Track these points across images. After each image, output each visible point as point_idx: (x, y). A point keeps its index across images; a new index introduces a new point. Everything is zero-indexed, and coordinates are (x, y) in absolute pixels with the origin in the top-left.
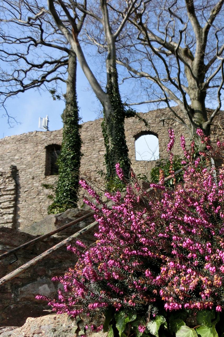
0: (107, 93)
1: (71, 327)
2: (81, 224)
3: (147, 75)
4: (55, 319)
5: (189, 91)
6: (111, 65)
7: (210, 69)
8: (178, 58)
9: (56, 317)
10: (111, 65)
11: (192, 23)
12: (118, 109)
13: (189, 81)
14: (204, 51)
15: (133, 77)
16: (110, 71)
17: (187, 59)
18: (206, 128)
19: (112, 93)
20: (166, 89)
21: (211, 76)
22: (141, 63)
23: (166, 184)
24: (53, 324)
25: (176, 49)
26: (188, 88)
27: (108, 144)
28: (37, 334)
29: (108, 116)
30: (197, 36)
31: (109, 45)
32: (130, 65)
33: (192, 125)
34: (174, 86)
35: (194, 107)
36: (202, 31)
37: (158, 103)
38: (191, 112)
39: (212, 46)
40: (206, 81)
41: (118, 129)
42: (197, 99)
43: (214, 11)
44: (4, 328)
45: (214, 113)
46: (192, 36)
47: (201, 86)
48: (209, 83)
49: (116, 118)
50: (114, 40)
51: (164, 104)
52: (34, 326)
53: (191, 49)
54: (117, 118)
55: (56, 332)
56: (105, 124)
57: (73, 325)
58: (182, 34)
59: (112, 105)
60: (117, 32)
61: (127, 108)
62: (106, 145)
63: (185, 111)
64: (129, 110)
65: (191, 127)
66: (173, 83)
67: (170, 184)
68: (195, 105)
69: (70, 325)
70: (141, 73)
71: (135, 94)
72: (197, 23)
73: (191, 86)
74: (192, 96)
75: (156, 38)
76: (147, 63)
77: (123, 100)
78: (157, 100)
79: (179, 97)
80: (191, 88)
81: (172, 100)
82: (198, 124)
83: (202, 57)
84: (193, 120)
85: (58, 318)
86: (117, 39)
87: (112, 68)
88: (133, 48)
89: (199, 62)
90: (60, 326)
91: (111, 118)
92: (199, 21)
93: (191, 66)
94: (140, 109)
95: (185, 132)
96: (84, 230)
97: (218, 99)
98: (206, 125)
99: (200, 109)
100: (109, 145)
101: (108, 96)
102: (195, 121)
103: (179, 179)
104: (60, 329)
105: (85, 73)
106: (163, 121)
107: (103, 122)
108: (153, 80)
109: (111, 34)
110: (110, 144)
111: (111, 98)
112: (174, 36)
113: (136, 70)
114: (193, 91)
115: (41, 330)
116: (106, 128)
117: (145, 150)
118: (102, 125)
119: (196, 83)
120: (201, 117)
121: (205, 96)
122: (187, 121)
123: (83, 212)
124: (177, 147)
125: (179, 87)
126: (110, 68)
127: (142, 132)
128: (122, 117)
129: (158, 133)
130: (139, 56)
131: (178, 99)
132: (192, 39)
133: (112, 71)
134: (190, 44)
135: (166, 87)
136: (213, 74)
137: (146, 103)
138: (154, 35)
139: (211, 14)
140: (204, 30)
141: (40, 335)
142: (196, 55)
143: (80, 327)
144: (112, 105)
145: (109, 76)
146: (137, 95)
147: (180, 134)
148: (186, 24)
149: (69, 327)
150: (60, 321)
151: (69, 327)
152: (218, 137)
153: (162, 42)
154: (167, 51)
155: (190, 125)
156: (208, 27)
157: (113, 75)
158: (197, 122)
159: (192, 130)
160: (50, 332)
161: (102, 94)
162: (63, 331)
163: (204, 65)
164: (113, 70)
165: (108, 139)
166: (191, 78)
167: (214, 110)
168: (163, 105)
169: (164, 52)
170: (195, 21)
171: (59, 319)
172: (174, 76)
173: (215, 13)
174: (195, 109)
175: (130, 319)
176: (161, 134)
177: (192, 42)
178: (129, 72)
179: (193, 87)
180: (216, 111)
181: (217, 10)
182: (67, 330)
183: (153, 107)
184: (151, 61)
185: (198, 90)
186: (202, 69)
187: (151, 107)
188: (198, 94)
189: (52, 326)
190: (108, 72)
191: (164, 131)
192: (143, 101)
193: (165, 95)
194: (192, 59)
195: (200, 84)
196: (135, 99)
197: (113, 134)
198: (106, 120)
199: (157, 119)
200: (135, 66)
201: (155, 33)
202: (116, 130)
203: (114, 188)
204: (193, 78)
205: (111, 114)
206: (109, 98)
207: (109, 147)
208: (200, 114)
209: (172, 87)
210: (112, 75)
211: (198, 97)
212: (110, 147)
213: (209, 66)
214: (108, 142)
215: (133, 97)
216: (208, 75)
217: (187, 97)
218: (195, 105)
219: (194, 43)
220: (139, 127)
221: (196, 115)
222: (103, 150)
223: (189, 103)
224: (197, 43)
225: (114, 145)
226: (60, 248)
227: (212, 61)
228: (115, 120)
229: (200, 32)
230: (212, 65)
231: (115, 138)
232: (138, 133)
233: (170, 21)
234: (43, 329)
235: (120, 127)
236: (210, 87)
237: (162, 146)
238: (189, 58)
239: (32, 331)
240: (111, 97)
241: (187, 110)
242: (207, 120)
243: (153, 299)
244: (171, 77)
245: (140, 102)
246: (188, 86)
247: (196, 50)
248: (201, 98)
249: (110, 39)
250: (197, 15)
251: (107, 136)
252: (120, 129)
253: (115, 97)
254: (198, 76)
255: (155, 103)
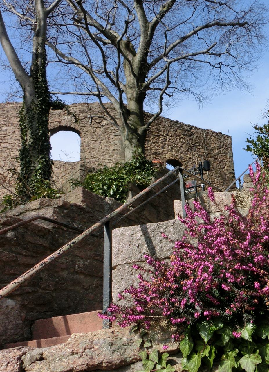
0: (31, 76)
1: (134, 340)
2: (8, 234)
3: (77, 62)
4: (113, 333)
5: (126, 89)
6: (39, 44)
7: (152, 70)
8: (120, 51)
9: (114, 331)
10: (39, 44)
11: (138, 14)
12: (42, 97)
13: (127, 78)
14: (149, 49)
15: (60, 61)
16: (37, 50)
17: (128, 53)
18: (142, 133)
19: (38, 78)
20: (99, 83)
21: (153, 77)
22: (71, 46)
23: (105, 193)
24: (111, 338)
25: (118, 39)
26: (125, 85)
27: (25, 138)
28: (89, 350)
29: (29, 103)
30: (142, 29)
31: (40, 19)
32: (58, 47)
33: (126, 129)
34: (109, 81)
35: (130, 108)
36: (148, 26)
37: (87, 96)
38: (126, 113)
39: (156, 44)
40: (147, 81)
41: (41, 121)
42: (134, 99)
43: (164, 7)
44: (22, 348)
45: (152, 118)
46: (135, 29)
47: (141, 86)
48: (150, 84)
49: (40, 108)
50: (47, 14)
51: (93, 99)
52: (85, 341)
53: (133, 43)
54: (41, 108)
55: (113, 346)
56: (24, 113)
57: (136, 338)
58: (129, 25)
59: (36, 92)
60: (51, 7)
61: (54, 98)
62: (22, 138)
63: (119, 111)
64: (57, 101)
65: (124, 130)
66: (108, 76)
67: (110, 194)
68: (132, 106)
69: (133, 338)
70: (70, 58)
71: (59, 81)
72: (144, 16)
73: (129, 84)
74: (129, 96)
75: (93, 22)
76: (78, 47)
77: (51, 89)
78: (86, 93)
79: (113, 94)
80: (129, 86)
81: (105, 96)
82: (133, 127)
83: (145, 54)
84: (128, 122)
85: (117, 332)
86: (50, 15)
87: (39, 48)
88: (64, 28)
89: (141, 59)
90: (119, 340)
91: (33, 107)
92: (147, 14)
93: (131, 62)
94: (68, 100)
95: (113, 134)
96: (74, 243)
97: (158, 103)
98: (142, 129)
99: (137, 111)
100: (27, 139)
101: (31, 79)
102: (130, 123)
103: (121, 189)
104: (118, 343)
105: (3, 47)
106: (92, 118)
107: (21, 110)
108: (85, 69)
109: (43, 7)
110: (28, 138)
111: (36, 83)
112: (113, 24)
113: (64, 53)
114: (130, 90)
115: (93, 345)
116: (25, 118)
117: (65, 148)
118: (20, 113)
119: (135, 81)
120: (137, 120)
121: (145, 98)
122: (120, 121)
123: (13, 219)
124: (102, 150)
125: (116, 84)
126: (37, 47)
127: (60, 126)
128: (47, 108)
129: (81, 131)
130: (70, 38)
131: (112, 96)
132: (134, 32)
133: (40, 51)
134: (131, 36)
135: (99, 80)
136: (155, 75)
137: (73, 94)
138: (91, 18)
139: (160, 10)
140: (150, 25)
141: (93, 350)
142: (139, 51)
143: (145, 340)
144: (36, 92)
145: (34, 56)
146: (62, 82)
147: (108, 136)
148: (134, 16)
149: (131, 340)
150: (119, 334)
151: (131, 340)
152: (151, 144)
153: (101, 28)
154: (104, 38)
155: (124, 127)
156: (156, 23)
157: (40, 57)
158: (132, 125)
159: (126, 133)
160: (106, 347)
161: (24, 76)
162: (123, 345)
163: (148, 64)
164: (42, 50)
165: (27, 131)
166: (130, 75)
167: (152, 115)
168: (94, 100)
169: (100, 39)
170: (142, 13)
171: (118, 333)
172: (111, 68)
173: (165, 9)
174: (131, 111)
175: (216, 327)
176: (84, 133)
177: (134, 35)
178: (56, 55)
179: (131, 86)
180: (155, 116)
181: (167, 7)
182: (128, 344)
183: (80, 99)
184: (85, 47)
185: (137, 89)
186: (144, 67)
187: (78, 101)
188: (137, 94)
189: (109, 340)
190: (34, 51)
191: (89, 129)
192: (67, 92)
193: (98, 89)
194: (134, 54)
195: (140, 84)
196: (59, 87)
197: (33, 126)
198: (25, 108)
199: (81, 114)
200: (64, 49)
201: (92, 16)
202: (38, 122)
203: (46, 193)
204: (132, 75)
205: (33, 102)
206: (33, 82)
207: (26, 141)
208: (136, 117)
209: (107, 81)
210: (39, 56)
211: (136, 98)
212: (28, 141)
213: (152, 64)
214: (26, 135)
215: (56, 85)
216: (150, 75)
217: (124, 95)
218: (132, 106)
219: (136, 35)
220: (58, 120)
221: (132, 118)
222: (6, 141)
223: (125, 102)
224: (142, 39)
225: (34, 139)
226: (52, 261)
227: (157, 61)
228: (38, 110)
229: (146, 26)
230: (156, 66)
231: (36, 131)
232: (56, 127)
233: (114, 8)
234: (96, 344)
235: (44, 119)
236: (151, 89)
237: (85, 146)
238: (130, 52)
239: (83, 346)
240: (35, 82)
241: (122, 110)
242: (143, 125)
243: (253, 308)
244: (108, 70)
245: (64, 92)
246: (125, 83)
247: (139, 45)
248: (140, 99)
249: (41, 13)
250: (144, 6)
251: (25, 128)
252: (43, 122)
253: (40, 82)
254: (139, 74)
255: (83, 96)
